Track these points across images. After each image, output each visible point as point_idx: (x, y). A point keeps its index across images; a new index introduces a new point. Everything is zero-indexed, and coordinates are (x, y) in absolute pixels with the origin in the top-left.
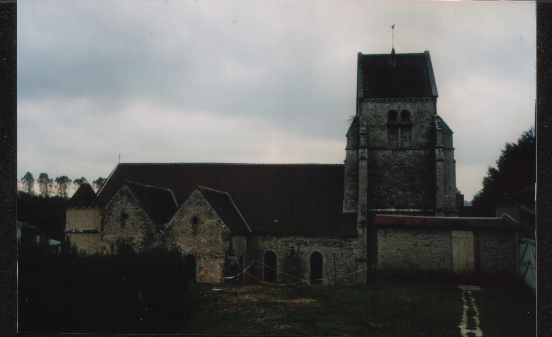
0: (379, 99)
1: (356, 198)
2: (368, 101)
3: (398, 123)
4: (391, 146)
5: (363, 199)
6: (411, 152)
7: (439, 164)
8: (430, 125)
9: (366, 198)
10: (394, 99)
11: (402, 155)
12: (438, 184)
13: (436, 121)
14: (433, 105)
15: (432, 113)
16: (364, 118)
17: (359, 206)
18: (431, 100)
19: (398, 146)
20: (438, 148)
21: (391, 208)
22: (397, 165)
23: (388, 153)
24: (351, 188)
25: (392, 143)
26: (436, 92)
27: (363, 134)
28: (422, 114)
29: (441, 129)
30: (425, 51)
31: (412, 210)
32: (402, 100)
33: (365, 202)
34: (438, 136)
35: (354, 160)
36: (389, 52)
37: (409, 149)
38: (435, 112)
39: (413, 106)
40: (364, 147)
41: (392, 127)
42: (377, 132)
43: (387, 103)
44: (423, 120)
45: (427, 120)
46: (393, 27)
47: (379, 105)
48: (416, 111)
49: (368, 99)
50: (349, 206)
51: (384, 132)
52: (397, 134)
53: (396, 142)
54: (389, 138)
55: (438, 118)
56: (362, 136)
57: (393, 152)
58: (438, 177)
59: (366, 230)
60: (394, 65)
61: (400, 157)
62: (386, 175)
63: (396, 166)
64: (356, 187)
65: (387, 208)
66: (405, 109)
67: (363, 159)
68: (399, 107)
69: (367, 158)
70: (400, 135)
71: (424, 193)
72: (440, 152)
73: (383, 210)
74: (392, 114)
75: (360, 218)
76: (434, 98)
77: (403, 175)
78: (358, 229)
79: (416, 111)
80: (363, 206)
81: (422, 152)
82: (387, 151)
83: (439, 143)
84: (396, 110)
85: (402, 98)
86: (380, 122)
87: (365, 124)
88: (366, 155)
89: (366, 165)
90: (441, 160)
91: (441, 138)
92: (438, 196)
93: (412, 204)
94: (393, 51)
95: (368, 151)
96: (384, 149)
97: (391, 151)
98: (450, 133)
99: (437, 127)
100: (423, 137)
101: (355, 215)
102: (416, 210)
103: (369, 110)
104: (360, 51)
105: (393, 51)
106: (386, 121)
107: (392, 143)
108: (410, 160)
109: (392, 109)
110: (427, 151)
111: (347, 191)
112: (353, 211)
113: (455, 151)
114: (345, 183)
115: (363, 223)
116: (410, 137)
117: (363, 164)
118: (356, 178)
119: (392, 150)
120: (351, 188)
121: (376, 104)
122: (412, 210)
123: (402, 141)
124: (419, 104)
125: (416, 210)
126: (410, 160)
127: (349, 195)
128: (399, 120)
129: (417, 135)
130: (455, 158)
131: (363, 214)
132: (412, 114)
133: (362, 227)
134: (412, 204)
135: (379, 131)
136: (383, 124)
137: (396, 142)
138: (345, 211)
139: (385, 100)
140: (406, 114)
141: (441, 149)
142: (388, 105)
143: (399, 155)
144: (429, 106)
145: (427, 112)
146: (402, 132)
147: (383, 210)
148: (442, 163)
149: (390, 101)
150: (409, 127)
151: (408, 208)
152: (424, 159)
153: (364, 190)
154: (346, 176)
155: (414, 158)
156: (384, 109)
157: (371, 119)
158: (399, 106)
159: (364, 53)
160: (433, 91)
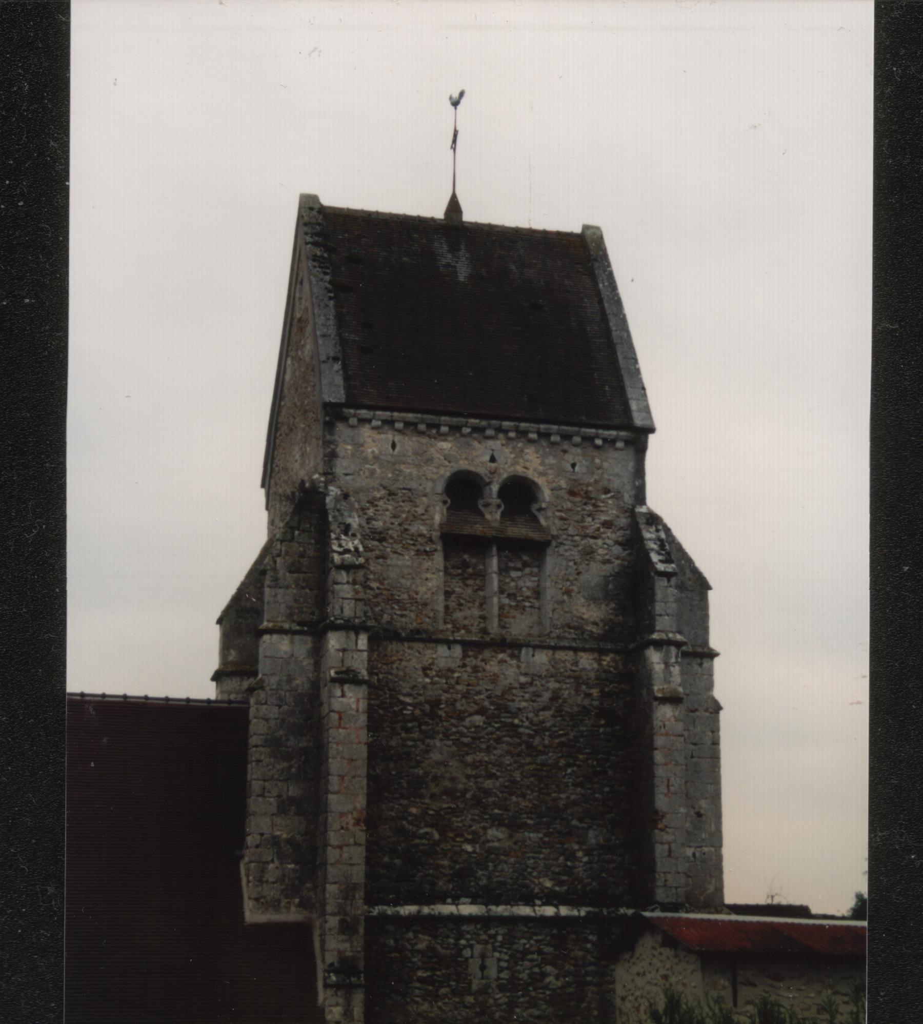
0: (410, 416)
1: (307, 856)
2: (363, 421)
3: (488, 529)
4: (456, 629)
5: (346, 855)
6: (541, 658)
7: (665, 714)
8: (617, 550)
9: (358, 854)
10: (472, 421)
11: (505, 670)
12: (661, 802)
13: (649, 534)
14: (631, 465)
15: (628, 498)
16: (346, 496)
17: (332, 889)
18: (628, 442)
19: (485, 631)
20: (659, 645)
21: (456, 901)
22: (482, 711)
23: (445, 656)
24: (282, 808)
25: (458, 615)
26: (647, 410)
27: (345, 567)
28: (588, 497)
29: (670, 568)
30: (586, 228)
31: (549, 911)
32: (506, 432)
33: (358, 874)
34: (659, 595)
35: (300, 682)
36: (436, 210)
37: (535, 647)
38: (640, 496)
39: (551, 460)
40: (349, 627)
41: (461, 547)
42: (401, 563)
43: (443, 436)
44: (592, 525)
45: (607, 524)
46: (455, 104)
47: (408, 444)
48: (563, 483)
49: (364, 413)
50: (271, 892)
51: (427, 564)
52: (482, 575)
53: (476, 612)
54: (448, 594)
55: (654, 519)
56: (343, 576)
57: (465, 656)
58: (660, 772)
59: (358, 998)
60: (463, 272)
61: (494, 679)
62: (436, 756)
63: (478, 719)
64: (311, 807)
65: (442, 899)
66: (519, 470)
67: (347, 677)
68: (493, 459)
69: (364, 674)
70: (495, 582)
71: (593, 837)
72: (667, 665)
73: (426, 910)
74: (463, 489)
75: (332, 946)
76: (637, 437)
77: (507, 760)
78: (322, 995)
79: (563, 483)
80: (348, 891)
81: (586, 661)
82: (442, 650)
83: (665, 625)
84: (481, 470)
85: (506, 424)
86: (415, 517)
87: (354, 521)
88: (360, 663)
89: (363, 705)
90: (674, 700)
91: (673, 607)
92: (660, 850)
93: (548, 884)
94: (454, 207)
95: (370, 640)
96: (422, 637)
97: (458, 651)
98: (701, 585)
99: (655, 557)
100: (592, 599)
101: (298, 938)
102: (564, 911)
103: (365, 460)
104: (310, 189)
105: (454, 207)
106: (438, 518)
107: (458, 615)
108: (537, 695)
109: (463, 465)
110: (607, 659)
111: (264, 821)
112: (293, 915)
113: (717, 661)
114: (256, 786)
115: (345, 967)
116: (538, 593)
117: (351, 701)
118: (311, 764)
119: (466, 645)
120: (282, 808)
121: (398, 438)
122: (549, 911)
123: (501, 608)
124: (575, 454)
125: (564, 911)
126: (537, 695)
127: (275, 842)
128: (493, 516)
129: (573, 586)
130: (718, 693)
131: (347, 928)
132: (547, 494)
133: (344, 989)
134: (548, 884)
135: (407, 559)
136: (424, 530)
137: (476, 612)
138: (252, 915)
139: (437, 426)
140: (519, 494)
141: (673, 650)
142: (445, 445)
143: (492, 667)
144: (614, 465)
145: (607, 491)
146: (503, 570)
147: (426, 910)
148: (679, 711)
149: (455, 429)
150: (534, 550)
151: (529, 900)
152: (595, 692)
153: (350, 820)
154: (254, 754)
155: (553, 685)
156: (430, 460)
157: (371, 503)
158: (499, 456)
159: (330, 199)
160: (634, 406)
